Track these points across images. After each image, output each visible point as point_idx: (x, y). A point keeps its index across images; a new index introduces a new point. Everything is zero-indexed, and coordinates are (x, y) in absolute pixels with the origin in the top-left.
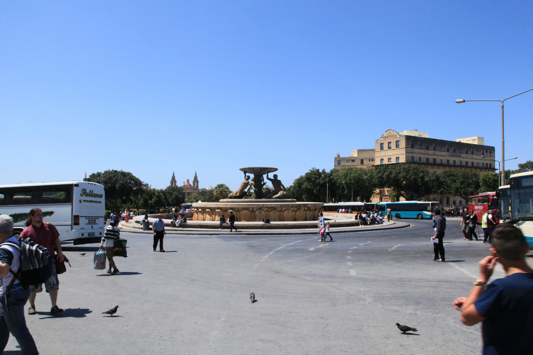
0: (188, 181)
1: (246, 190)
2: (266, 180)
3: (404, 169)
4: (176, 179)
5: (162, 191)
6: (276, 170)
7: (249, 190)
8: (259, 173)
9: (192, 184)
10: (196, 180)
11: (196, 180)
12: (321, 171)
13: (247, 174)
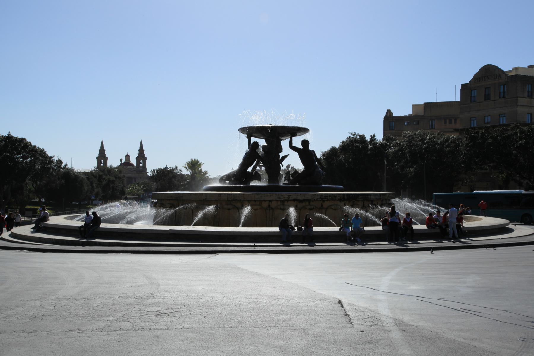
0: (128, 156)
1: (250, 170)
2: (286, 149)
3: (522, 132)
4: (107, 154)
5: (85, 173)
6: (305, 130)
7: (255, 168)
8: (275, 134)
9: (135, 164)
10: (141, 156)
11: (141, 156)
12: (368, 138)
13: (253, 140)
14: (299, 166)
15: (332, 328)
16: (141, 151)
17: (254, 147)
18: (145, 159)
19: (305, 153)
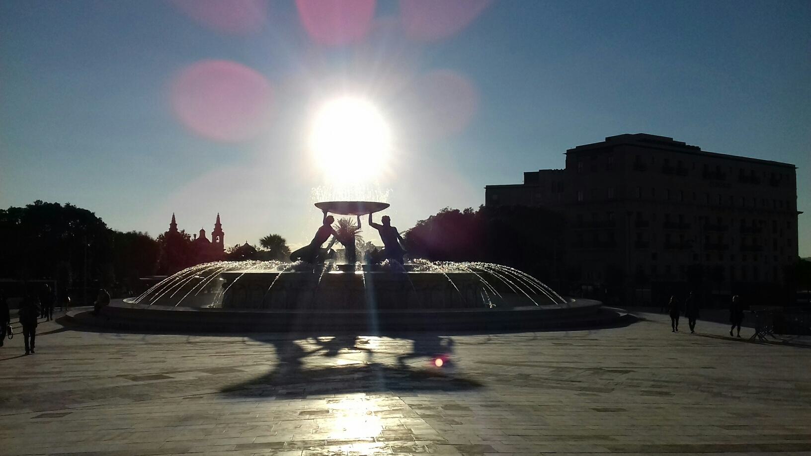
6: (384, 206)
11: (218, 231)
13: (329, 214)
14: (378, 242)
15: (200, 440)
16: (218, 225)
17: (328, 221)
18: (222, 235)
19: (386, 230)
